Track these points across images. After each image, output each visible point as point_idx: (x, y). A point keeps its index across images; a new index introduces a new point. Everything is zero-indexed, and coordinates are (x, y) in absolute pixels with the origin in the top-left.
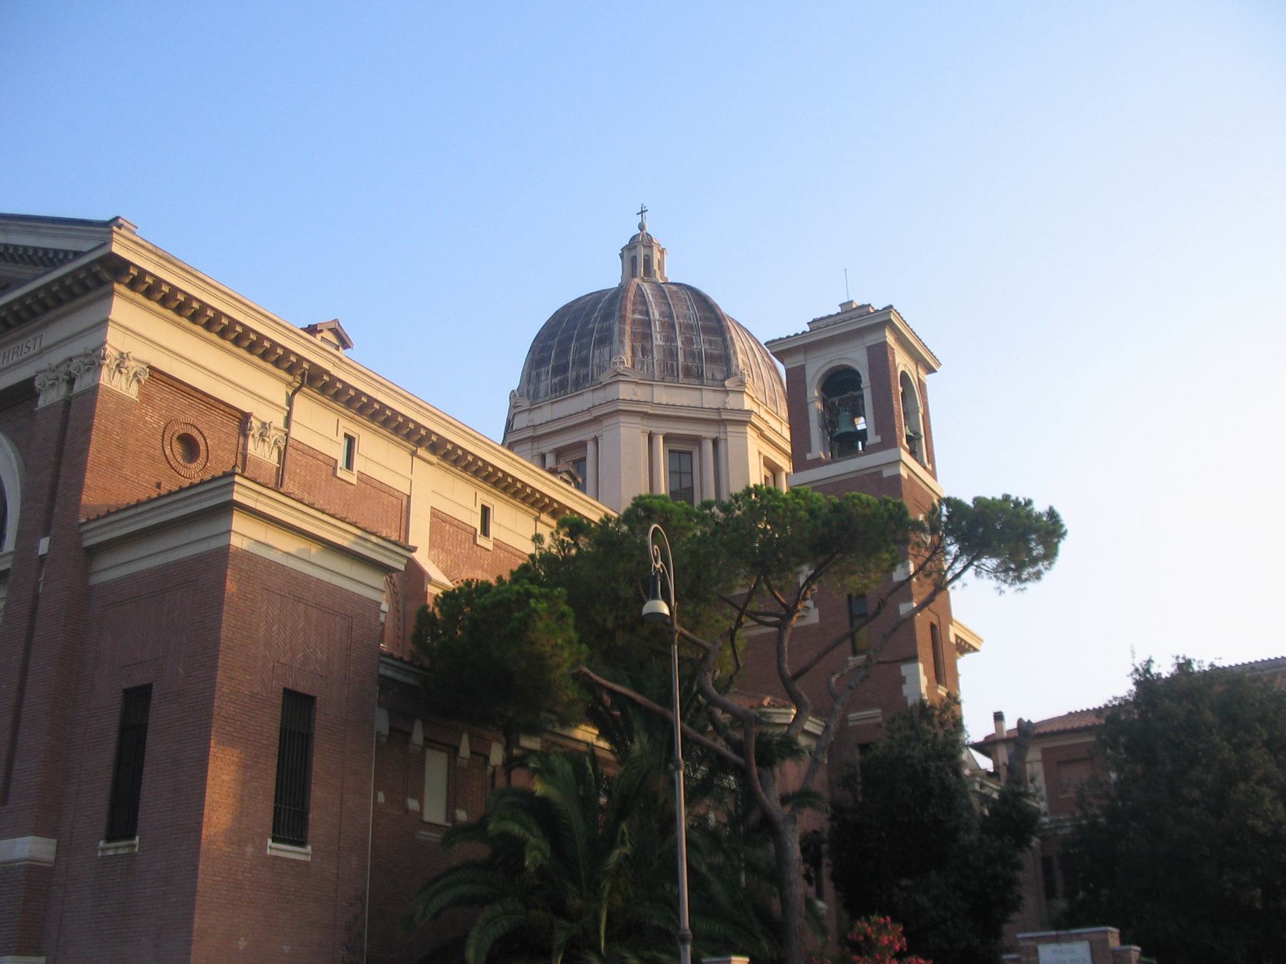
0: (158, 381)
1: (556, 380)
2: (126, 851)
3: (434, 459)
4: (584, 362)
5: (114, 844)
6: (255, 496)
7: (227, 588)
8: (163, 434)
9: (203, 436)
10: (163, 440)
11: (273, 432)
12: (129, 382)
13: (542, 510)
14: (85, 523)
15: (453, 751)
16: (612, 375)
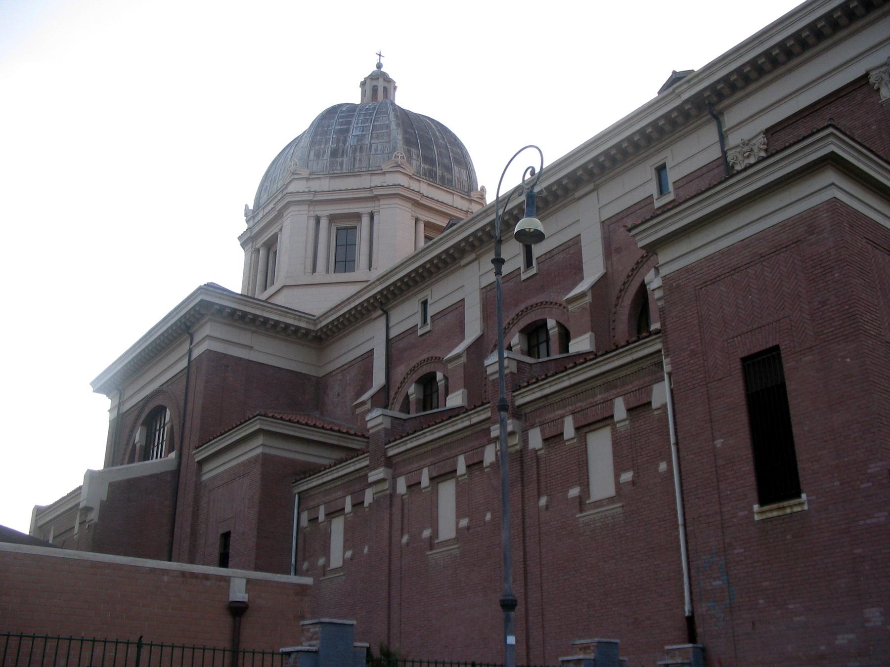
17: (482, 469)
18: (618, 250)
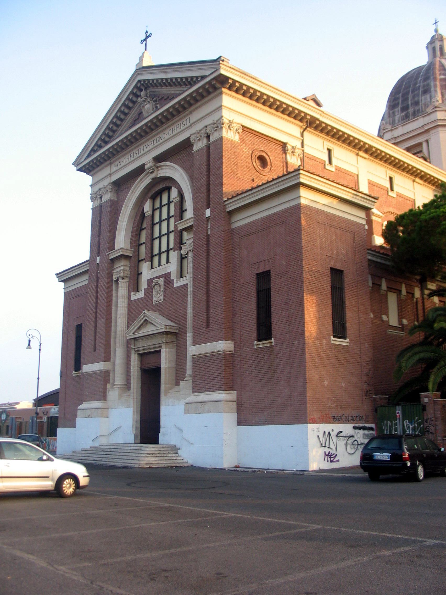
0: (246, 132)
1: (403, 114)
2: (268, 345)
3: (366, 156)
4: (417, 103)
5: (262, 342)
6: (309, 179)
7: (302, 223)
8: (252, 156)
9: (268, 155)
10: (252, 159)
11: (297, 150)
12: (235, 133)
13: (416, 176)
14: (226, 201)
15: (399, 292)
16: (433, 108)
17: (190, 154)
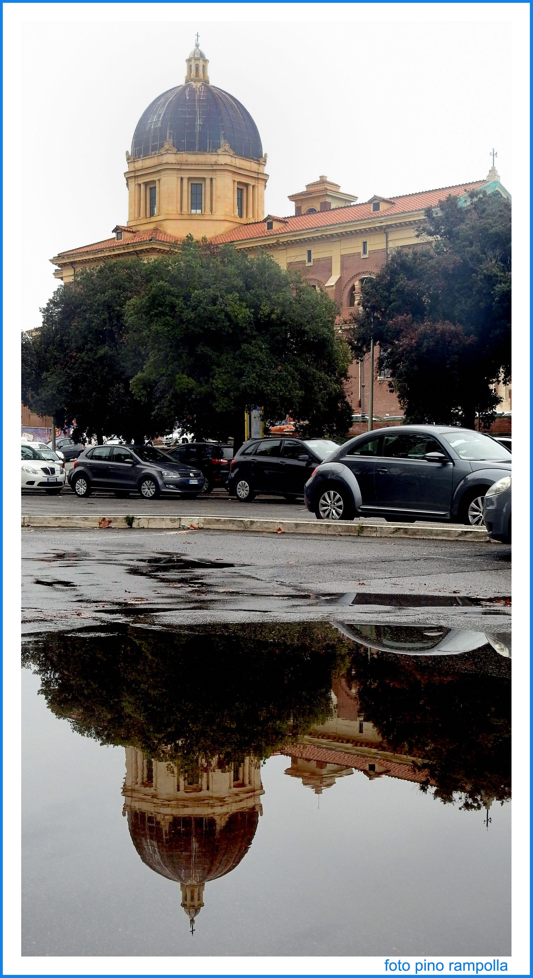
18: (346, 268)
